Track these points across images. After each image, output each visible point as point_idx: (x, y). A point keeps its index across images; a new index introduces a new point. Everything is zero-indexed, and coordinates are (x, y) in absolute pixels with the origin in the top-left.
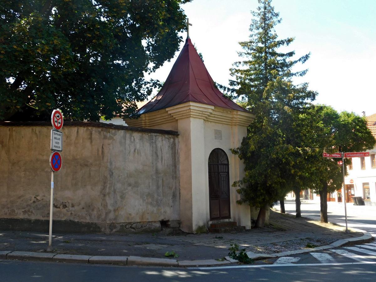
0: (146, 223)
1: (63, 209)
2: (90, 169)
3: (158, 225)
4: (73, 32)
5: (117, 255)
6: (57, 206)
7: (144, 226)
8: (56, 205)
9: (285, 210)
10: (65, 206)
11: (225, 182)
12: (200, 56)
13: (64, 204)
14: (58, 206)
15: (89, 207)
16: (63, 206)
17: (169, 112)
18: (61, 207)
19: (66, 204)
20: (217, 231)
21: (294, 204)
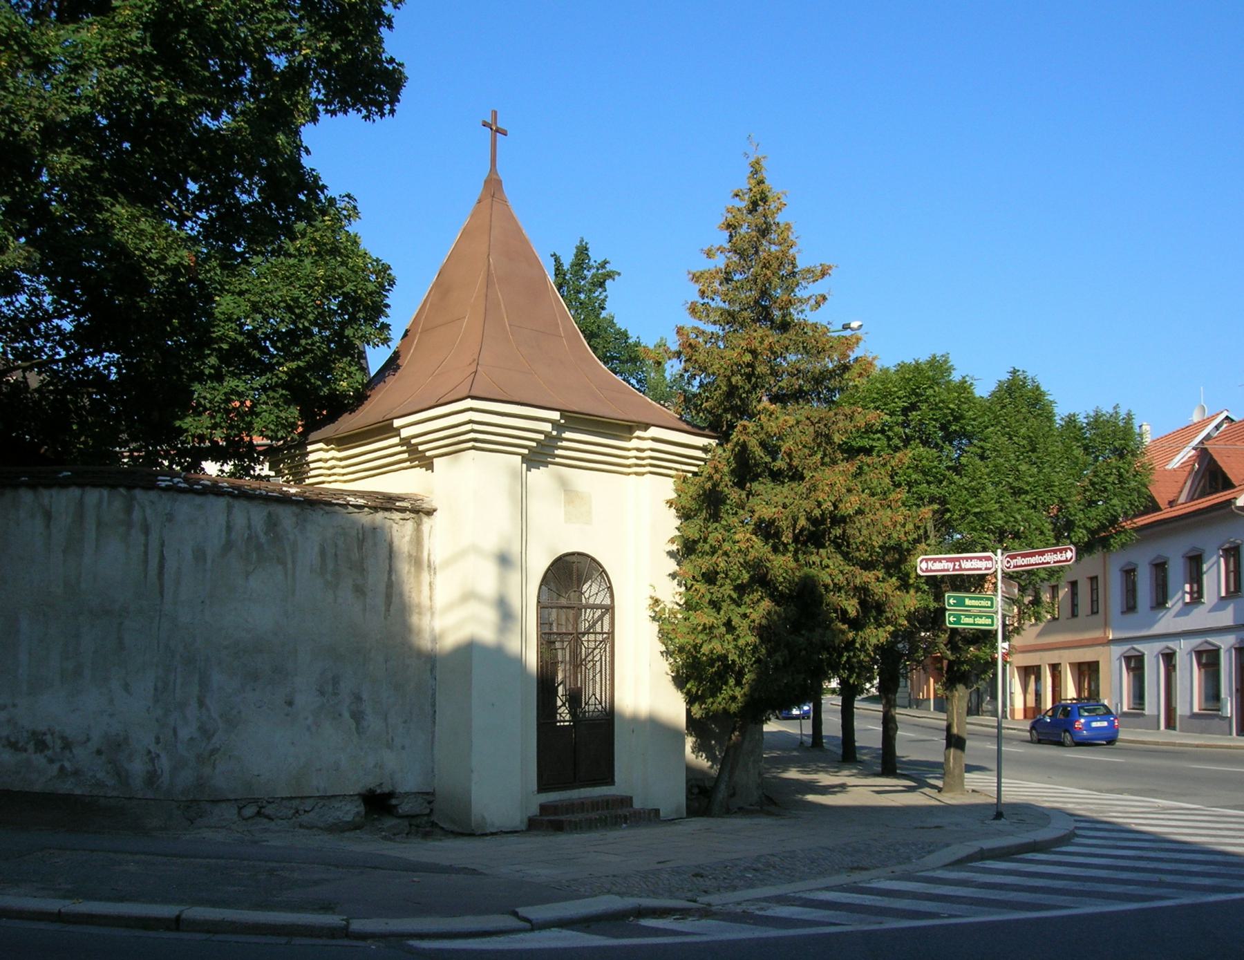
0: (311, 801)
1: (36, 752)
2: (121, 624)
3: (351, 811)
4: (99, 397)
5: (108, 899)
6: (17, 742)
7: (305, 811)
8: (13, 740)
9: (824, 734)
10: (41, 745)
11: (950, 565)
12: (320, 429)
13: (40, 737)
14: (20, 745)
15: (115, 746)
16: (36, 744)
17: (405, 433)
18: (31, 747)
19: (44, 738)
20: (558, 827)
21: (857, 708)
